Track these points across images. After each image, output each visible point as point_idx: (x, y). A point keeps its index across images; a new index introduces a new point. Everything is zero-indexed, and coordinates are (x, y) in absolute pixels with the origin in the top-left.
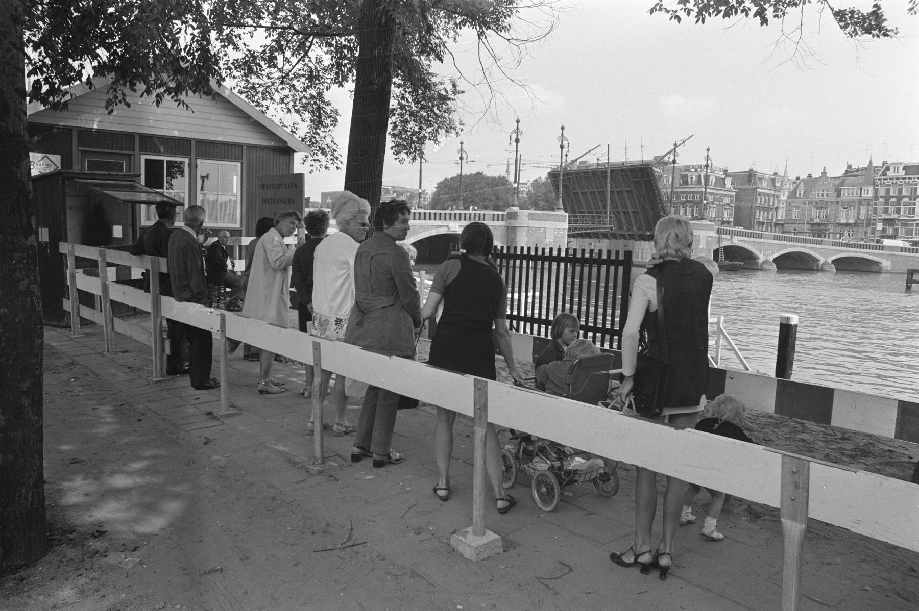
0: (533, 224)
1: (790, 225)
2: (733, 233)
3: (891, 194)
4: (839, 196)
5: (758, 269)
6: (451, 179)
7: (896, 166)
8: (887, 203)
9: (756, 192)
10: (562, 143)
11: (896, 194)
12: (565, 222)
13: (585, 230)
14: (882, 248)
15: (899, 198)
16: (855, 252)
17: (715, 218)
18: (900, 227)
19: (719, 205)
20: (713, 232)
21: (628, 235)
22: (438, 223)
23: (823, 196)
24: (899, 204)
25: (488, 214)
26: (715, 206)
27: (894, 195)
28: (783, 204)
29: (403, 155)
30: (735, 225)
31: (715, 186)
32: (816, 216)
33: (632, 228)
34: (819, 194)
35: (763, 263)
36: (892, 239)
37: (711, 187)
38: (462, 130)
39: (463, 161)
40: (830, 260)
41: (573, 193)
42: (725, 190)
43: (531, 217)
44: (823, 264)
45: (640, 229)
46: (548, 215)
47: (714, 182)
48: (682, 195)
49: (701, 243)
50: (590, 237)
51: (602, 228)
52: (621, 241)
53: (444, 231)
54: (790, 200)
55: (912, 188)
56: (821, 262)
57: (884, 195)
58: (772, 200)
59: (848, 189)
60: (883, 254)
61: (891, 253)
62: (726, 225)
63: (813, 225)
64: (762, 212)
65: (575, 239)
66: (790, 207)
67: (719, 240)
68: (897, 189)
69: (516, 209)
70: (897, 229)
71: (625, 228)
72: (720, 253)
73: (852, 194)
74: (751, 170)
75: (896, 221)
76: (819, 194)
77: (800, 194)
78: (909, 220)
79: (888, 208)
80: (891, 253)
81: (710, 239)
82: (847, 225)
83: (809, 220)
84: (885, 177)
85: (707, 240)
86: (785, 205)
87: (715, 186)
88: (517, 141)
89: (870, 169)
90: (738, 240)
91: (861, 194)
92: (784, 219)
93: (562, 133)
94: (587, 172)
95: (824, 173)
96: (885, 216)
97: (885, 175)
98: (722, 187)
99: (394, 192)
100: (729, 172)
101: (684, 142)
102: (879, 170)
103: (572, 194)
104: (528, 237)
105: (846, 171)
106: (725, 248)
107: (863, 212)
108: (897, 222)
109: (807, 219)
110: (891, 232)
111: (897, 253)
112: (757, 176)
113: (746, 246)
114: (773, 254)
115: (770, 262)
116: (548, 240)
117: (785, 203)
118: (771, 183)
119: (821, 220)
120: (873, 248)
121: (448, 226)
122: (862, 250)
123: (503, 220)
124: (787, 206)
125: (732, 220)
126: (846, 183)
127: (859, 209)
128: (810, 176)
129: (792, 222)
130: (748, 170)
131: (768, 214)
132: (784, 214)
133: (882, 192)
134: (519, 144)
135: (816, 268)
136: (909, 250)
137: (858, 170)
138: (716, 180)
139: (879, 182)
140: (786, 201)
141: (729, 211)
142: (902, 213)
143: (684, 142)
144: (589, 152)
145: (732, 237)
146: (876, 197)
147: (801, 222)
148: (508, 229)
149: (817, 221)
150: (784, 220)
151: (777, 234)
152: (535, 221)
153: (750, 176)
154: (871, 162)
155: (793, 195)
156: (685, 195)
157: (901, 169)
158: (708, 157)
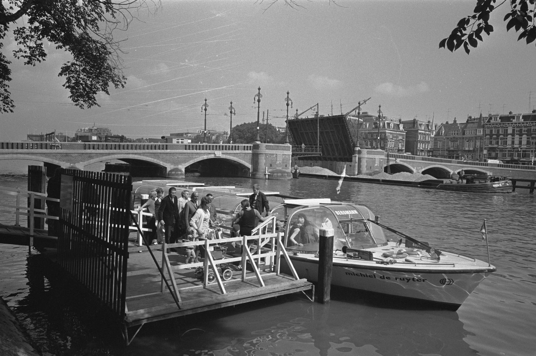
1: (436, 152)
2: (396, 157)
4: (464, 134)
6: (241, 125)
7: (496, 116)
8: (491, 138)
9: (418, 132)
11: (496, 133)
12: (290, 150)
13: (304, 155)
14: (487, 165)
15: (498, 135)
17: (394, 147)
18: (499, 152)
19: (396, 140)
20: (384, 156)
21: (333, 158)
22: (209, 151)
23: (455, 134)
24: (498, 139)
26: (394, 140)
27: (495, 133)
30: (406, 152)
32: (451, 146)
33: (335, 154)
34: (452, 133)
36: (493, 159)
37: (391, 129)
38: (125, 83)
39: (289, 106)
40: (456, 172)
42: (399, 132)
43: (268, 148)
44: (452, 175)
45: (340, 154)
46: (278, 146)
48: (374, 134)
49: (376, 163)
50: (311, 160)
51: (315, 154)
52: (329, 162)
53: (212, 156)
54: (436, 137)
55: (505, 130)
56: (451, 174)
58: (427, 137)
59: (469, 130)
61: (492, 167)
63: (449, 151)
64: (421, 144)
67: (388, 160)
69: (258, 142)
70: (497, 154)
71: (331, 154)
72: (388, 169)
73: (472, 133)
74: (415, 120)
76: (452, 133)
77: (442, 133)
78: (503, 148)
79: (492, 141)
80: (492, 167)
81: (381, 160)
82: (469, 151)
83: (447, 148)
84: (489, 123)
85: (380, 161)
86: (433, 140)
87: (393, 129)
88: (206, 110)
90: (400, 161)
91: (476, 133)
92: (433, 148)
93: (288, 96)
94: (308, 121)
95: (455, 121)
96: (490, 146)
99: (209, 133)
100: (402, 121)
101: (365, 102)
102: (486, 119)
103: (300, 134)
104: (266, 160)
105: (468, 120)
106: (391, 165)
107: (478, 144)
108: (497, 149)
110: (494, 155)
111: (495, 168)
112: (418, 123)
114: (422, 169)
118: (426, 127)
119: (454, 148)
121: (214, 153)
122: (475, 166)
123: (250, 150)
124: (434, 140)
125: (404, 149)
127: (476, 142)
128: (447, 123)
129: (437, 150)
131: (425, 145)
132: (433, 145)
133: (488, 132)
134: (260, 103)
135: (448, 177)
136: (502, 166)
137: (474, 119)
138: (394, 125)
139: (486, 126)
141: (402, 143)
142: (500, 144)
144: (311, 108)
145: (396, 159)
148: (254, 155)
149: (452, 149)
150: (433, 149)
152: (270, 150)
153: (414, 122)
154: (481, 114)
155: (438, 134)
156: (376, 134)
158: (380, 111)
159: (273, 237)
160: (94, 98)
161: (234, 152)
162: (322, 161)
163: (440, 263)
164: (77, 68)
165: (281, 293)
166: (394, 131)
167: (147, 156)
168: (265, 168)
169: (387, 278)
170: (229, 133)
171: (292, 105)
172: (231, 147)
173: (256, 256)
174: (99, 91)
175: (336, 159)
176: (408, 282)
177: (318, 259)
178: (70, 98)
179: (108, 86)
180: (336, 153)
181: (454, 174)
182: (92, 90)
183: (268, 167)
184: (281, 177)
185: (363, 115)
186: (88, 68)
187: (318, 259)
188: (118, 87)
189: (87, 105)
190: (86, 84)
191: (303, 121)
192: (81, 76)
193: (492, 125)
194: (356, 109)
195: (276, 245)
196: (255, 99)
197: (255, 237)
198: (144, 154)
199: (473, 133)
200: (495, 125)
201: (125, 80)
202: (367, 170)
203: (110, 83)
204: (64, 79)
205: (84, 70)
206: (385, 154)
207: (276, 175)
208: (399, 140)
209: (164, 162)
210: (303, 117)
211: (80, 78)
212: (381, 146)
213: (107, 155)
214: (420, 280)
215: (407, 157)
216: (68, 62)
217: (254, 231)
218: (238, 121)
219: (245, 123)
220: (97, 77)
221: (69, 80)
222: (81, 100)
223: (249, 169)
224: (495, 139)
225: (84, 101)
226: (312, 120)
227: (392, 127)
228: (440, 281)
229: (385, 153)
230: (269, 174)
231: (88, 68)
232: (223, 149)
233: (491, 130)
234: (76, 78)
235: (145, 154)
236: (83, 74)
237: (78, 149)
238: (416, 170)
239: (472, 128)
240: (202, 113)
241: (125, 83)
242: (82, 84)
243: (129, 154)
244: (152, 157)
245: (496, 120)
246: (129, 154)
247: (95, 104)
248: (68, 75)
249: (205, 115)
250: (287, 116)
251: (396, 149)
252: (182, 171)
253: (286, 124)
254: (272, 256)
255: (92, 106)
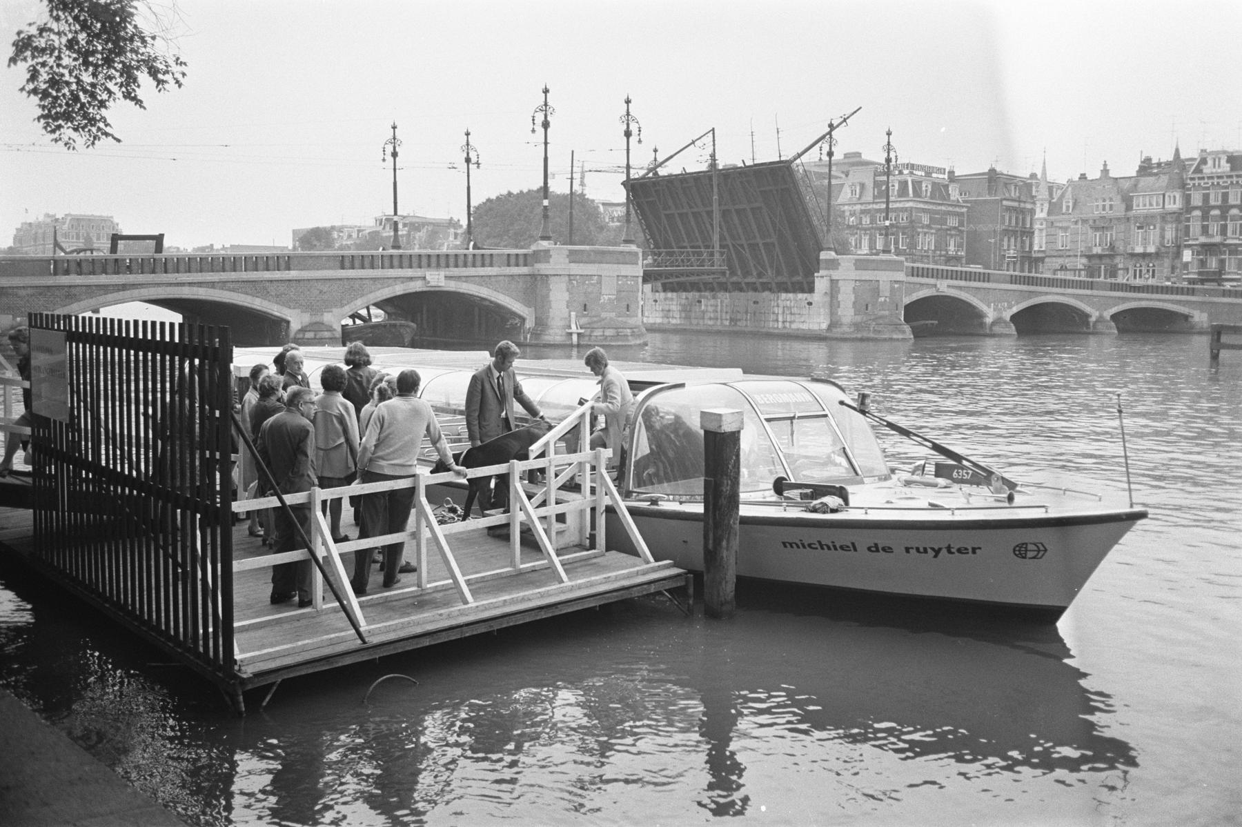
0: (577, 269)
3: (1212, 203)
4: (1129, 208)
5: (1090, 333)
7: (1216, 155)
8: (1205, 217)
10: (889, 155)
11: (1219, 203)
12: (637, 264)
13: (677, 277)
16: (1147, 299)
18: (1227, 256)
22: (409, 272)
25: (498, 255)
26: (933, 231)
27: (1216, 204)
28: (1042, 224)
29: (67, 132)
30: (969, 262)
31: (931, 198)
35: (994, 323)
37: (926, 200)
38: (184, 74)
40: (1107, 314)
41: (665, 215)
45: (779, 273)
47: (930, 190)
48: (878, 215)
53: (417, 286)
54: (1052, 218)
56: (1093, 319)
57: (1200, 204)
60: (1194, 302)
62: (952, 263)
63: (1090, 257)
65: (675, 294)
66: (1053, 229)
68: (1220, 195)
74: (992, 171)
75: (1221, 247)
81: (896, 286)
82: (1144, 255)
84: (1200, 175)
87: (931, 198)
88: (546, 125)
89: (1178, 163)
90: (949, 286)
92: (1043, 249)
93: (628, 110)
95: (1105, 171)
96: (1203, 240)
97: (1201, 171)
98: (945, 199)
100: (956, 175)
101: (845, 120)
103: (663, 217)
104: (570, 294)
109: (1081, 248)
113: (964, 296)
114: (1010, 307)
115: (1005, 322)
116: (606, 297)
117: (1044, 223)
119: (1103, 250)
120: (1081, 285)
126: (1140, 186)
127: (1163, 229)
128: (1083, 177)
130: (987, 171)
132: (1044, 242)
133: (1197, 200)
137: (1159, 165)
139: (1191, 183)
140: (1045, 219)
142: (1229, 233)
143: (845, 120)
144: (693, 142)
146: (1188, 208)
147: (1071, 253)
149: (1097, 250)
151: (1016, 273)
154: (1177, 151)
157: (1223, 162)
159: (585, 462)
160: (103, 119)
161: (481, 271)
162: (730, 292)
163: (1014, 505)
164: (53, 41)
165: (609, 598)
166: (934, 204)
167: (233, 290)
168: (570, 316)
169: (884, 549)
170: (464, 223)
171: (639, 135)
172: (470, 259)
173: (543, 511)
174: (114, 100)
175: (766, 287)
176: (936, 556)
177: (699, 508)
178: (39, 121)
179: (139, 86)
180: (769, 271)
181: (1100, 319)
182: (97, 99)
183: (577, 312)
184: (615, 341)
185: (846, 161)
186: (83, 40)
187: (699, 508)
188: (165, 89)
189: (85, 138)
190: (79, 82)
191: (671, 179)
192: (66, 61)
193: (1225, 179)
194: (823, 137)
195: (594, 485)
196: (533, 120)
197: (540, 463)
198: (223, 285)
199: (1155, 204)
200: (1215, 181)
201: (183, 68)
202: (855, 315)
203: (143, 77)
204: (22, 69)
205: (71, 44)
206: (907, 268)
207: (601, 334)
208: (949, 230)
209: (283, 304)
210: (671, 169)
211: (64, 67)
212: (897, 248)
213: (119, 290)
214: (966, 549)
215: (968, 276)
216: (30, 25)
217: (535, 448)
218: (487, 189)
219: (510, 194)
220: (108, 62)
221: (34, 75)
222: (68, 128)
223: (523, 320)
224: (1215, 218)
225: (76, 130)
226: (697, 177)
227: (929, 194)
228: (1014, 550)
229: (906, 264)
230: (582, 331)
231: (83, 40)
232: (447, 266)
233: (1204, 194)
234: (51, 67)
235: (228, 285)
236: (70, 57)
237: (33, 275)
238: (994, 310)
239: (1152, 191)
240: (384, 165)
241: (184, 74)
242: (68, 84)
243: (182, 284)
244: (247, 293)
245: (1219, 166)
246: (182, 284)
247: (107, 134)
248: (29, 59)
249: (395, 170)
250: (628, 167)
251: (940, 256)
252: (335, 330)
253: (624, 192)
254: (585, 510)
255: (96, 142)
